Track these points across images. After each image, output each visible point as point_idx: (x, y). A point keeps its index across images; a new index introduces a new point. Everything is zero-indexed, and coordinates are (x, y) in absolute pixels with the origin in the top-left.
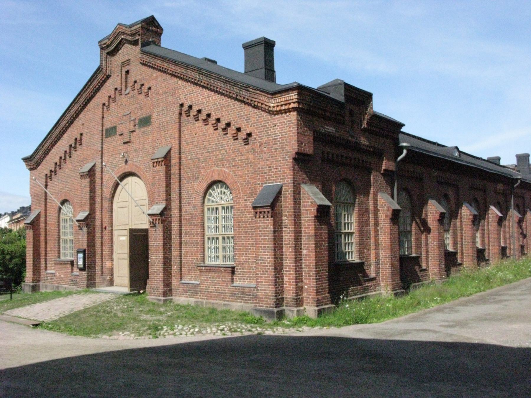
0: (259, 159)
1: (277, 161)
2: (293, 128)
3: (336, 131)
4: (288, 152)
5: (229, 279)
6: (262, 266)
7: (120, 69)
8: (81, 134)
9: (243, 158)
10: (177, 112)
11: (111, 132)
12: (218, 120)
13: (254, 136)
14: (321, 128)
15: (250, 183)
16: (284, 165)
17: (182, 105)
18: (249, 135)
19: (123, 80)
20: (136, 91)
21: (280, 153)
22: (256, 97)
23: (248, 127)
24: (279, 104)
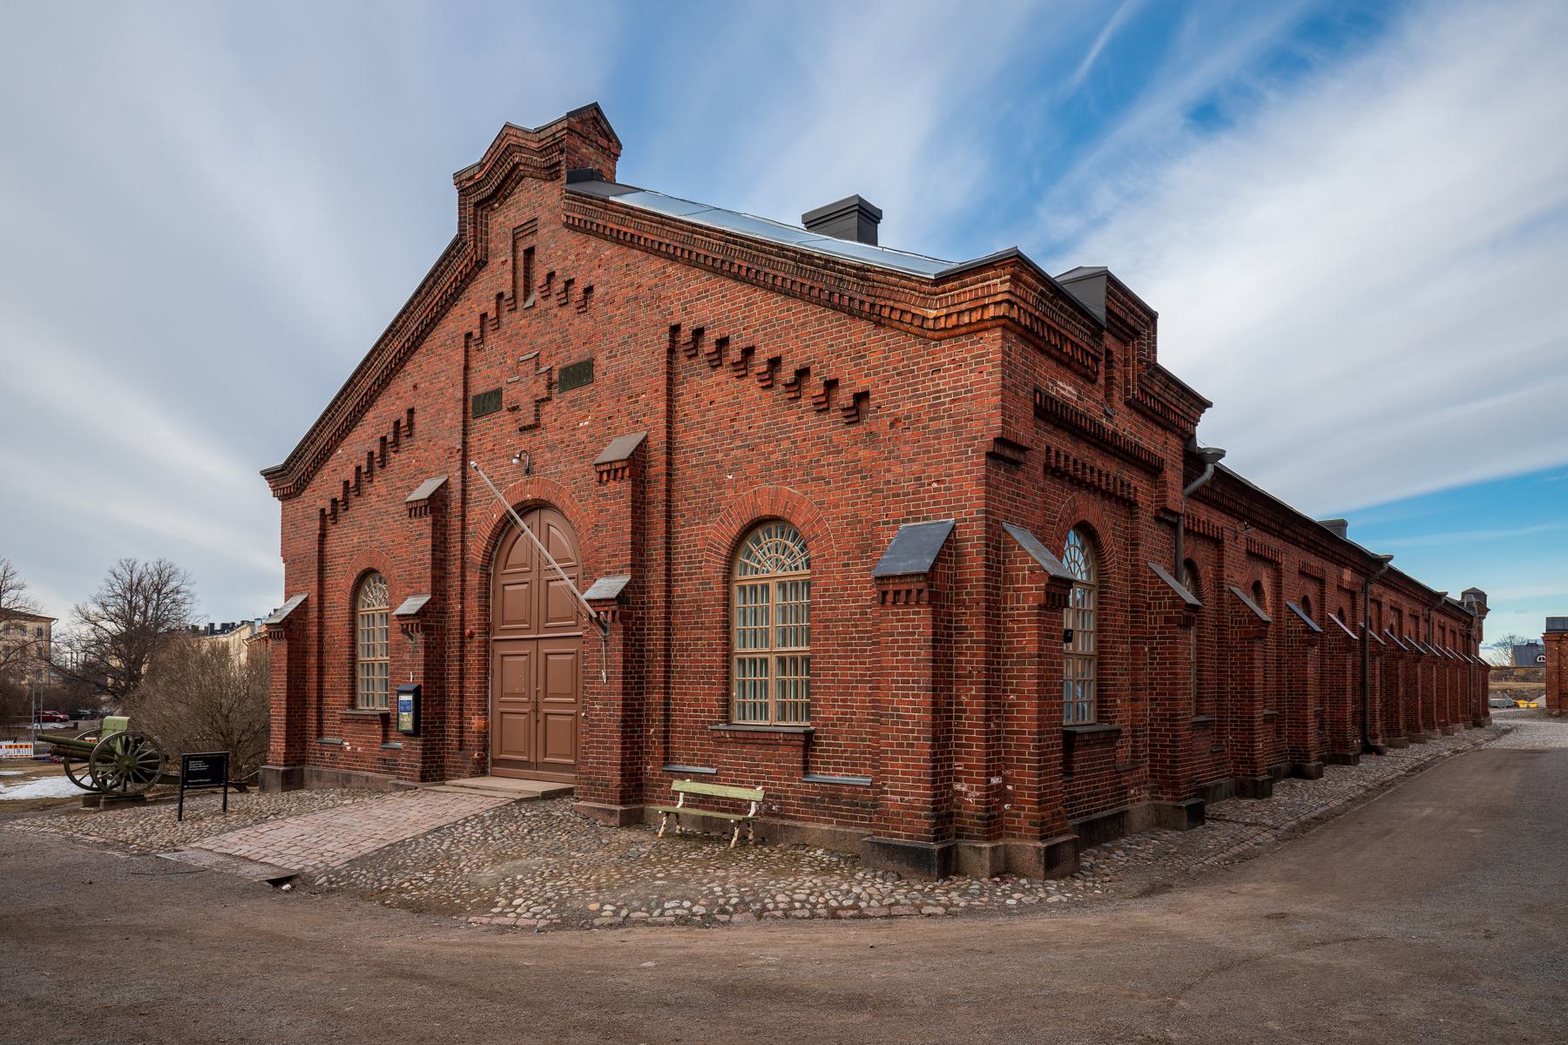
1: (939, 463)
4: (975, 438)
5: (379, 738)
6: (898, 730)
8: (411, 412)
9: (841, 458)
11: (480, 405)
13: (875, 399)
15: (860, 522)
16: (960, 473)
17: (675, 329)
18: (861, 397)
20: (553, 301)
22: (886, 294)
24: (952, 310)
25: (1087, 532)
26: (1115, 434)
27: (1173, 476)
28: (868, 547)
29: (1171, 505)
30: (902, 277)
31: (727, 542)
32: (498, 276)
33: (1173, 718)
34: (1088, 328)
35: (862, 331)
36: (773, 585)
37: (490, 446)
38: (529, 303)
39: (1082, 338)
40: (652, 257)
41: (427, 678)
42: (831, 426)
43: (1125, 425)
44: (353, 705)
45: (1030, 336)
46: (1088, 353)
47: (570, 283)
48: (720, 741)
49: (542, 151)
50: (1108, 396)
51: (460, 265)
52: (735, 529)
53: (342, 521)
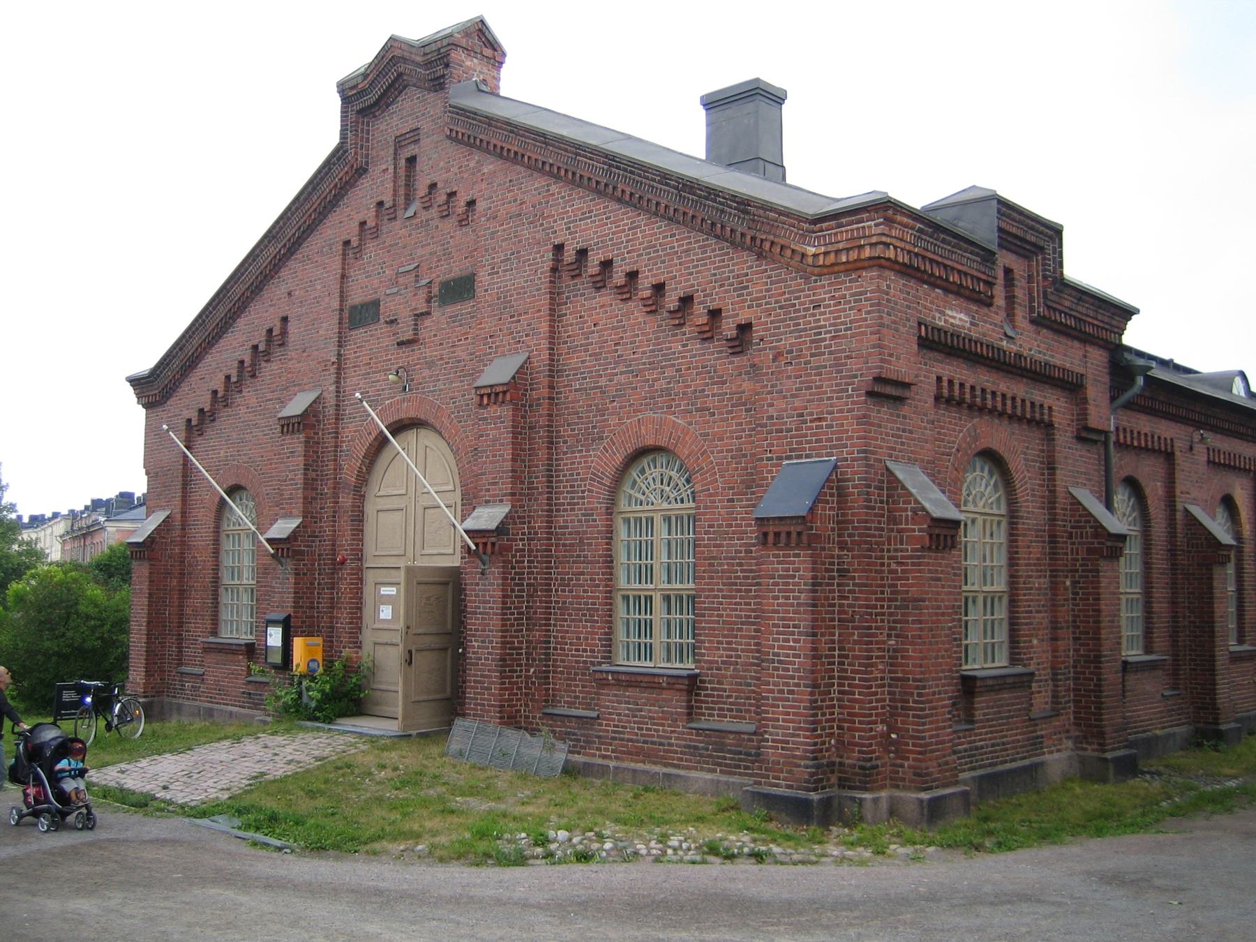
1: (821, 400)
2: (868, 312)
3: (972, 324)
7: (391, 151)
8: (285, 320)
9: (726, 388)
10: (547, 266)
11: (360, 315)
12: (659, 288)
14: (937, 315)
15: (745, 456)
16: (841, 411)
17: (559, 248)
18: (745, 328)
19: (402, 182)
20: (434, 212)
21: (830, 379)
23: (742, 308)
24: (830, 248)
25: (992, 458)
26: (1019, 356)
27: (1097, 393)
28: (752, 484)
29: (1093, 422)
30: (781, 213)
31: (610, 472)
32: (378, 184)
33: (1097, 659)
34: (977, 254)
35: (744, 263)
36: (658, 519)
37: (366, 359)
38: (410, 213)
39: (969, 263)
40: (536, 174)
41: (296, 606)
42: (714, 355)
43: (1031, 344)
44: (215, 633)
45: (909, 271)
46: (979, 279)
47: (452, 194)
48: (603, 684)
49: (428, 64)
50: (1010, 315)
51: (339, 173)
52: (619, 458)
53: (209, 433)
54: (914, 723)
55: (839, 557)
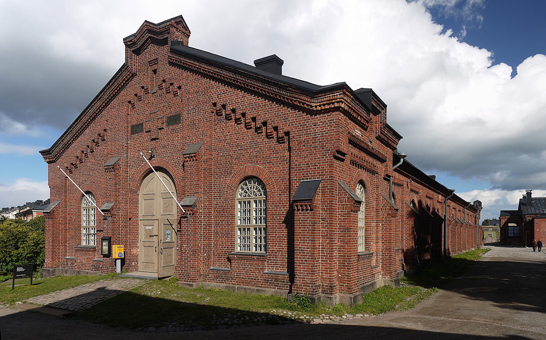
0: (297, 156)
11: (136, 129)
17: (215, 104)
18: (287, 134)
24: (321, 103)
25: (361, 182)
43: (376, 146)
54: (347, 271)
55: (322, 214)
